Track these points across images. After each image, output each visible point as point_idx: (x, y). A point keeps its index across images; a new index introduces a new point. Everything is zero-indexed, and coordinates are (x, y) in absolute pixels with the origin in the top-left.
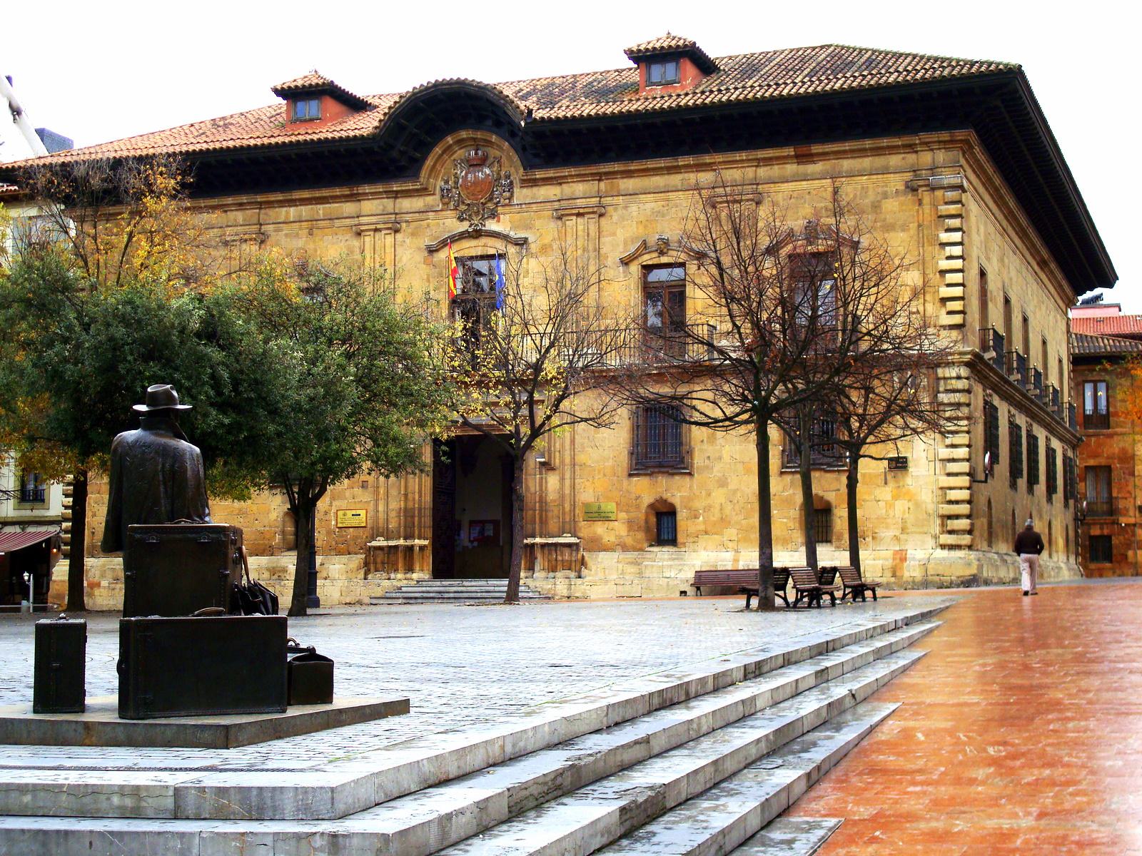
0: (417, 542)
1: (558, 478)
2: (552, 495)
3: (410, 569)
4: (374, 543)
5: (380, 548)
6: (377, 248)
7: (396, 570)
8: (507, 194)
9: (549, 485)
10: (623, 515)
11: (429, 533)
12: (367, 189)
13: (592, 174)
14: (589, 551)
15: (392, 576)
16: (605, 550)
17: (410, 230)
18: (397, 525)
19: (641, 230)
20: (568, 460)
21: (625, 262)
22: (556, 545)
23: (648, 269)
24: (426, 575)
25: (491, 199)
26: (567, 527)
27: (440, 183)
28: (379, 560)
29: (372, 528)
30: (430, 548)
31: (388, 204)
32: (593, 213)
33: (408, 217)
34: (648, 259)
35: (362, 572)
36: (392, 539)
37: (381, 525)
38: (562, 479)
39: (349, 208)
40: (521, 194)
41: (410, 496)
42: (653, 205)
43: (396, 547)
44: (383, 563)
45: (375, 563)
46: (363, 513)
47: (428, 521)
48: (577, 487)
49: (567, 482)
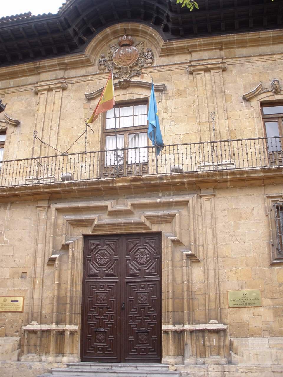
0: (68, 327)
1: (202, 269)
2: (197, 285)
3: (60, 352)
4: (29, 327)
5: (34, 332)
6: (48, 101)
7: (47, 353)
8: (150, 61)
9: (194, 275)
10: (267, 302)
11: (79, 319)
12: (46, 63)
13: (216, 44)
14: (236, 336)
15: (44, 358)
16: (252, 336)
17: (74, 88)
18: (49, 311)
19: (256, 78)
20: (211, 253)
21: (247, 99)
22: (203, 331)
23: (264, 104)
24: (75, 358)
25: (136, 65)
26: (213, 314)
27: (99, 58)
28: (32, 342)
29: (28, 313)
30: (79, 333)
31: (60, 74)
32: (218, 68)
33: (73, 80)
34: (265, 97)
35: (16, 353)
36: (45, 323)
37: (35, 311)
38: (206, 271)
39: (32, 79)
40: (158, 61)
41: (63, 286)
42: (263, 63)
43: (48, 331)
44: (35, 346)
45: (29, 345)
46: (20, 300)
47: (78, 308)
48: (221, 277)
49: (211, 273)
